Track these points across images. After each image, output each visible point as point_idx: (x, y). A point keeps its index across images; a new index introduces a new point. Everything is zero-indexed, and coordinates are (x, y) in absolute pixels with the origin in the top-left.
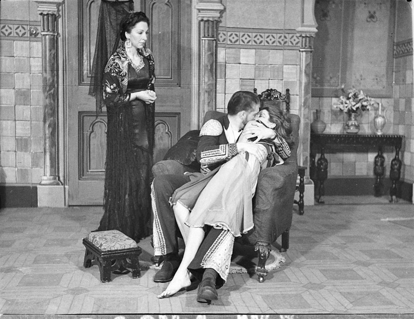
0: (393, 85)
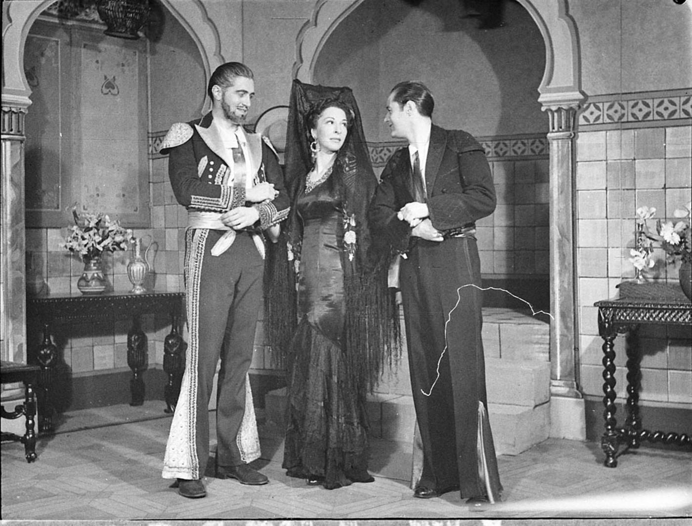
0: (151, 205)
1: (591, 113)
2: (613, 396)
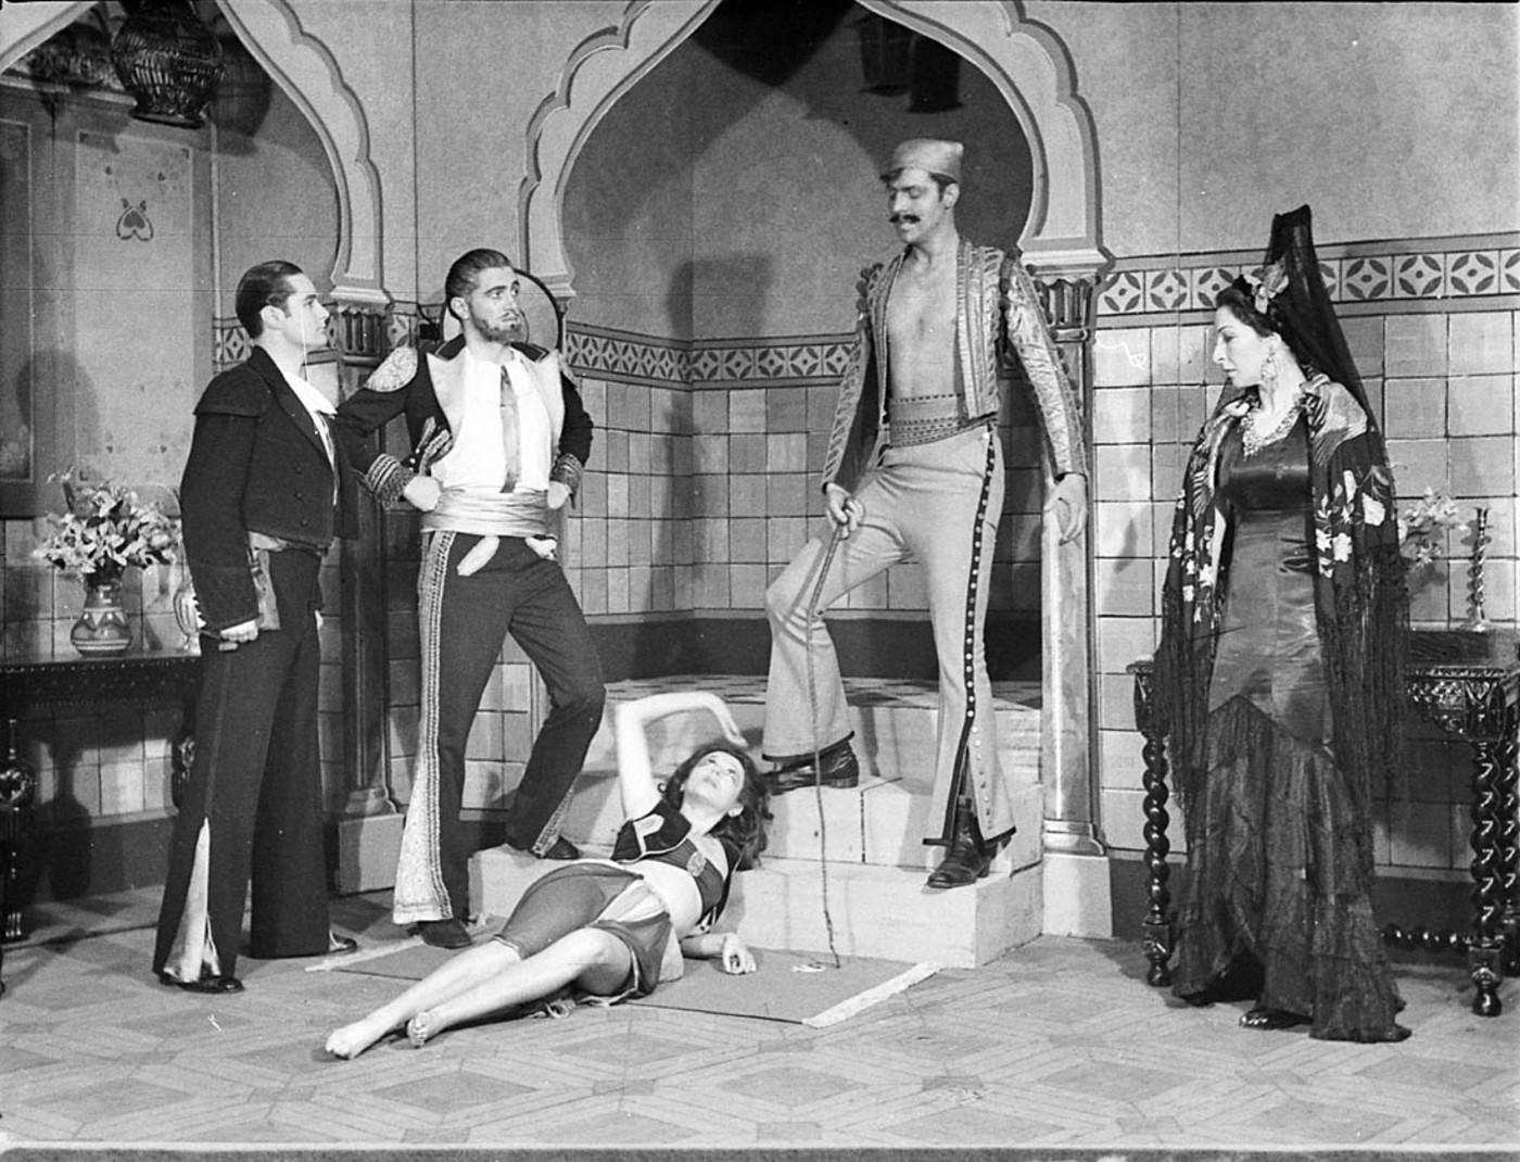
1: (1119, 293)
2: (1162, 847)
